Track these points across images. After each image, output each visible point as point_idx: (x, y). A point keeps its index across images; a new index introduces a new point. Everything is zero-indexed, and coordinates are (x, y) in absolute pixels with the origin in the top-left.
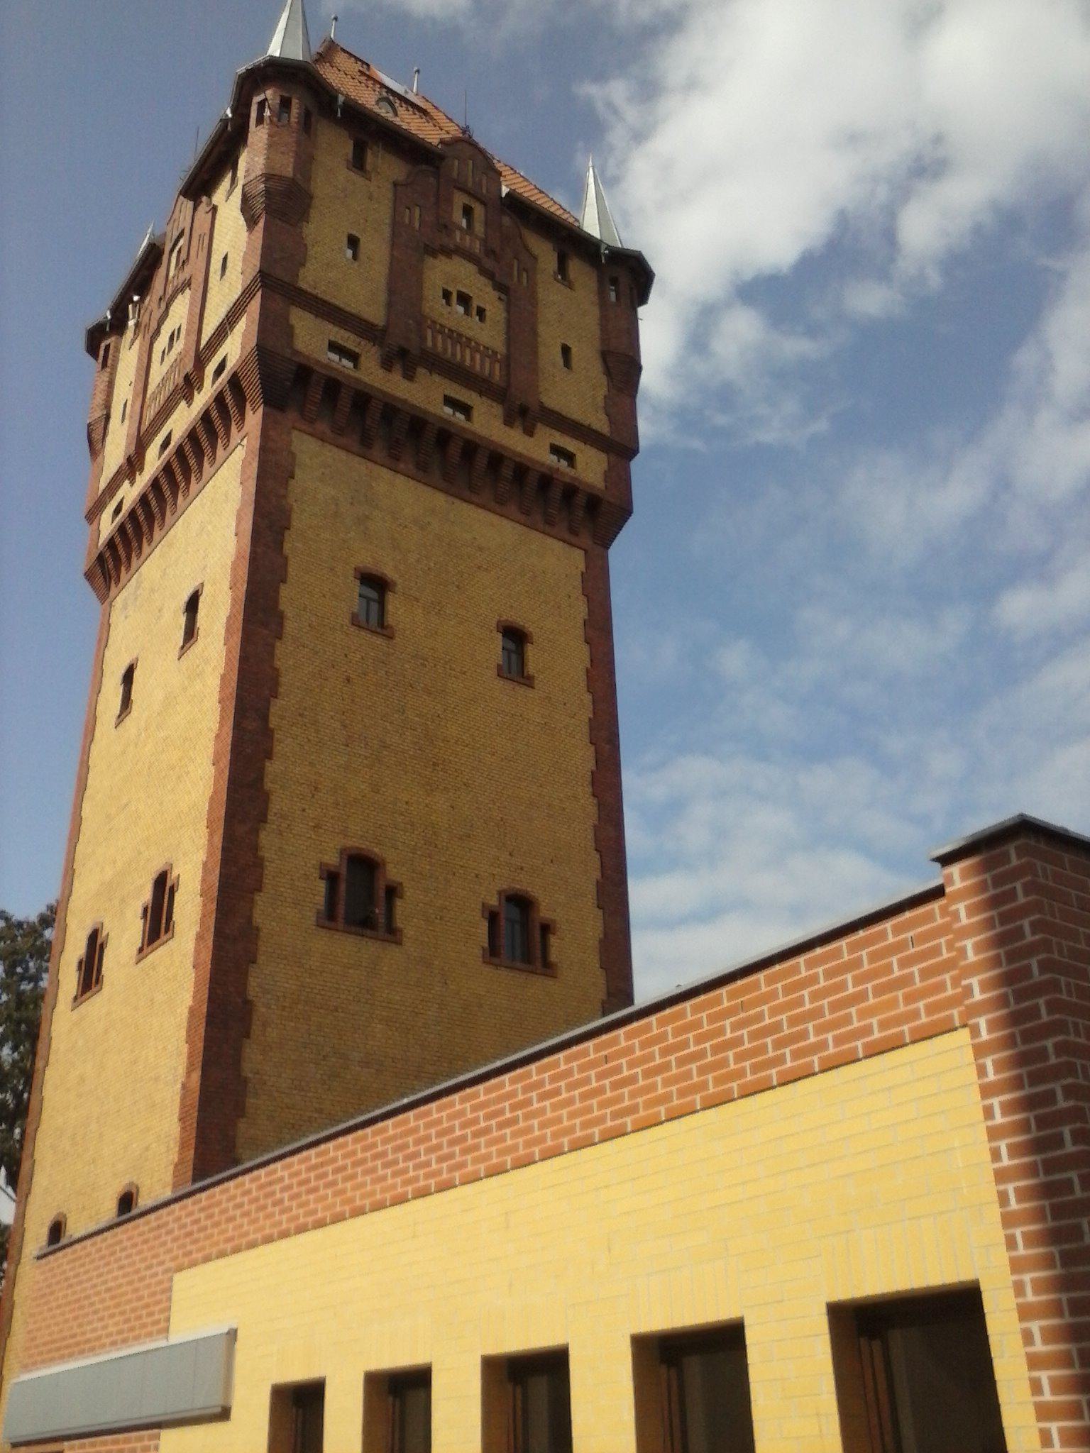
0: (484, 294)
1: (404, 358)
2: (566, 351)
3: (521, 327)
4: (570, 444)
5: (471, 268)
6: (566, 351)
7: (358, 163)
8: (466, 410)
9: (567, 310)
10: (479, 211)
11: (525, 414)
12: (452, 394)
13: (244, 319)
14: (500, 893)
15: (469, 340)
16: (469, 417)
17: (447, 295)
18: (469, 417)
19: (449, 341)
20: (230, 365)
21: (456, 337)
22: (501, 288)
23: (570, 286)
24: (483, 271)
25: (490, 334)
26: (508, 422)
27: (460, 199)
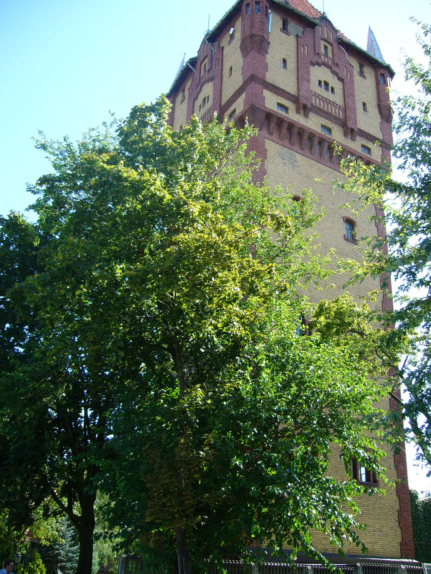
0: (333, 82)
1: (304, 109)
2: (364, 104)
3: (348, 94)
4: (369, 145)
5: (328, 71)
6: (364, 104)
7: (284, 29)
8: (329, 130)
9: (364, 86)
10: (329, 48)
11: (351, 132)
12: (366, 144)
13: (244, 93)
14: (12, 212)
15: (333, 103)
16: (287, 112)
17: (320, 82)
18: (287, 112)
19: (317, 99)
20: (238, 112)
21: (325, 100)
22: (341, 80)
23: (364, 77)
24: (333, 72)
25: (337, 98)
26: (345, 135)
27: (323, 43)
